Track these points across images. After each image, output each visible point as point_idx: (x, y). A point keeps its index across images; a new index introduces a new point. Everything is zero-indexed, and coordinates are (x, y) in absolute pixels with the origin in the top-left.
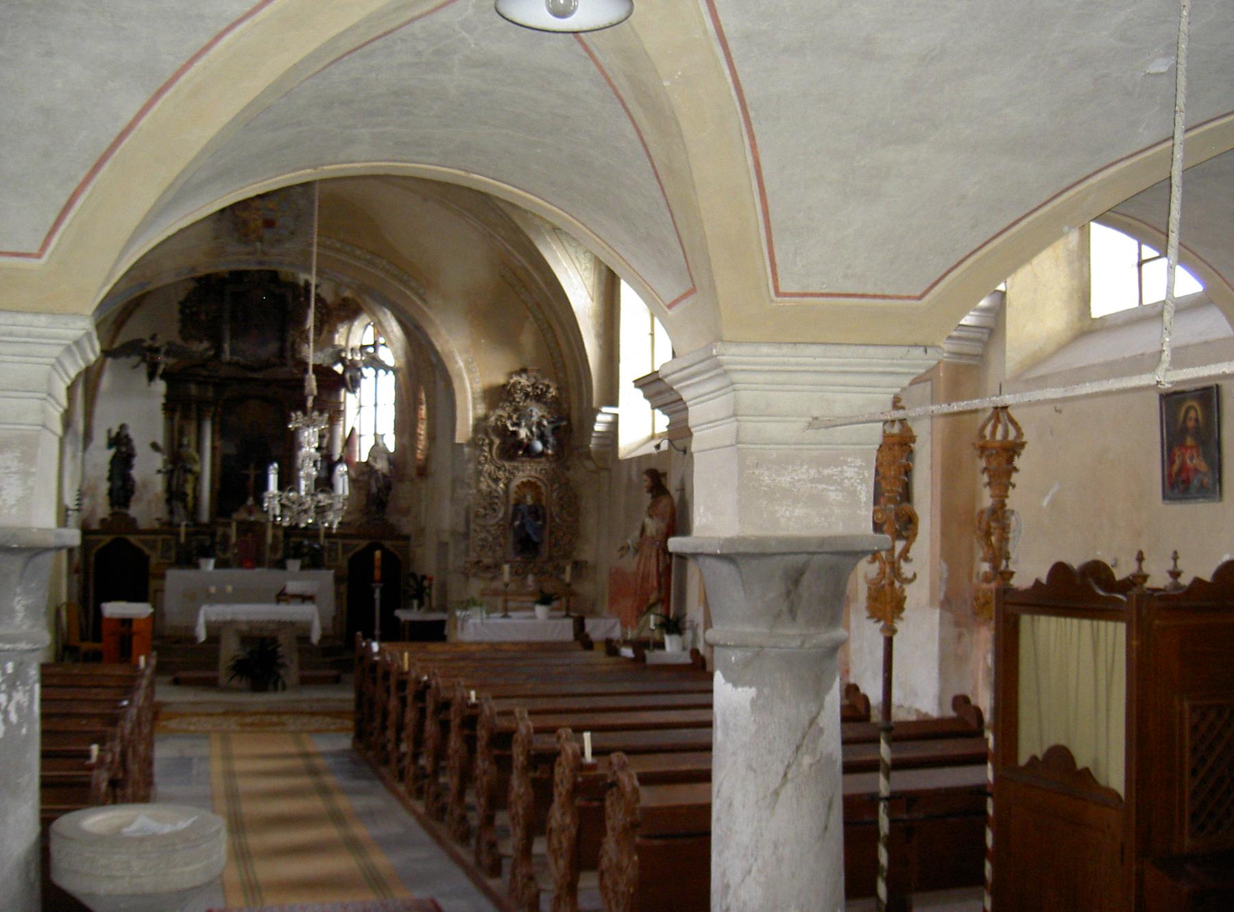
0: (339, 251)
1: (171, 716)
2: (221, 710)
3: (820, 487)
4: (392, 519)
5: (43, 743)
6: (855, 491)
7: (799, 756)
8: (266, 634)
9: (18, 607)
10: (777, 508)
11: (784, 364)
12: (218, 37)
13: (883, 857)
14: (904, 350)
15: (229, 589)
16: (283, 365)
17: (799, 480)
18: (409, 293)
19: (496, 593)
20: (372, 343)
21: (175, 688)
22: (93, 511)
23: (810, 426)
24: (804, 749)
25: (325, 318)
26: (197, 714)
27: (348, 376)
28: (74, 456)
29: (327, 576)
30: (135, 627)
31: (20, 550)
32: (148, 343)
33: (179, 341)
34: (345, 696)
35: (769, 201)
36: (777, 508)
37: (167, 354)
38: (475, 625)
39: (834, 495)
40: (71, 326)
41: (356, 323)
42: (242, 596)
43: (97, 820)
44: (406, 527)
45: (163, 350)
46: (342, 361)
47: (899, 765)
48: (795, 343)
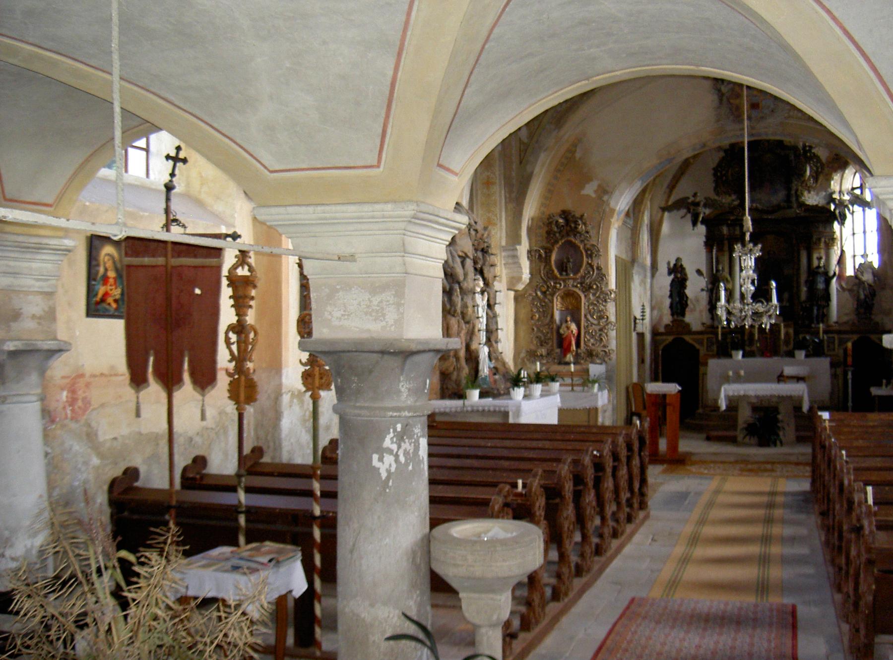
1: (694, 463)
2: (732, 459)
9: (403, 390)
12: (409, 14)
15: (742, 373)
16: (790, 207)
20: (859, 185)
22: (661, 318)
25: (820, 170)
27: (837, 212)
28: (643, 282)
29: (823, 364)
30: (668, 401)
32: (691, 199)
33: (714, 196)
34: (807, 450)
37: (705, 206)
40: (406, 209)
41: (847, 171)
42: (753, 377)
45: (702, 203)
46: (833, 200)
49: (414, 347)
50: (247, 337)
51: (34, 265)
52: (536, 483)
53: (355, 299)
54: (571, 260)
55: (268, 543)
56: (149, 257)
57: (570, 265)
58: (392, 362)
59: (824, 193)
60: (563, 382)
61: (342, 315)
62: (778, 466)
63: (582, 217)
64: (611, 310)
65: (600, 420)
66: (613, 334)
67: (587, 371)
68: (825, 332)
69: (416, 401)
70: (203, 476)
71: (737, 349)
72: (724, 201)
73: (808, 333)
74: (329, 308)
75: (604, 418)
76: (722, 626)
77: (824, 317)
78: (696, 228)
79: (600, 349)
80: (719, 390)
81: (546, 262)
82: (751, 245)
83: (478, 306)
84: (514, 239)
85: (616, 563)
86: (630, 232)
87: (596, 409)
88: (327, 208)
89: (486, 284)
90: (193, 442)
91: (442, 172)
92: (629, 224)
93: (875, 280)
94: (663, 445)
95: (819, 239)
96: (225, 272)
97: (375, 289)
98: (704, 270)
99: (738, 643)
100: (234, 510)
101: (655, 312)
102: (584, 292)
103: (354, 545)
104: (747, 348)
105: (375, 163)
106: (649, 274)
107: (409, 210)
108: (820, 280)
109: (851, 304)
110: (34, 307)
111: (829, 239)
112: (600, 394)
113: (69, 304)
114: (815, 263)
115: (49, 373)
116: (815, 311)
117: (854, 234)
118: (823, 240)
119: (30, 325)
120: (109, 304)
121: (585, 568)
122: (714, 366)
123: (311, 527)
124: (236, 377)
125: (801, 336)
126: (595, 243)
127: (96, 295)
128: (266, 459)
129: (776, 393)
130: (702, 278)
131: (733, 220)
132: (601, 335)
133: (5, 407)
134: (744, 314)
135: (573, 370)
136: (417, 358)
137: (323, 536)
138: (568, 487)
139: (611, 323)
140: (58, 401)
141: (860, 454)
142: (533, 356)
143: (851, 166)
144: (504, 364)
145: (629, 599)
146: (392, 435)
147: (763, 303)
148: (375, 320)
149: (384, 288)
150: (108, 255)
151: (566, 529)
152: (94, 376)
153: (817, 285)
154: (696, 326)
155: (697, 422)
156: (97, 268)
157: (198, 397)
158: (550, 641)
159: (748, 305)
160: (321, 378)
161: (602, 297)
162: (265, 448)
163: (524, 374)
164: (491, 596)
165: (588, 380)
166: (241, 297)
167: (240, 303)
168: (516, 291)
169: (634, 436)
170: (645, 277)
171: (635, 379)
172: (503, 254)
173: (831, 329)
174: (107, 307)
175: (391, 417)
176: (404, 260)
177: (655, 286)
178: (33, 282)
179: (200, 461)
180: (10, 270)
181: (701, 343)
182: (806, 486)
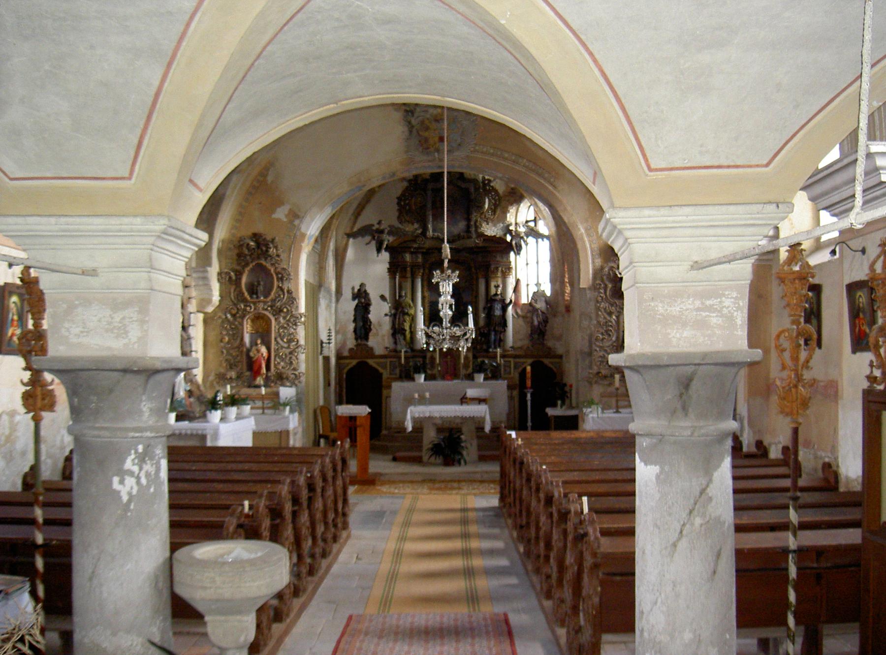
0: (493, 155)
1: (383, 483)
2: (420, 478)
3: (704, 314)
4: (550, 343)
5: (170, 498)
6: (732, 316)
7: (692, 518)
8: (454, 426)
9: (144, 409)
10: (669, 331)
11: (665, 222)
12: (188, 25)
13: (792, 596)
14: (760, 207)
15: (427, 395)
16: (470, 237)
17: (687, 310)
18: (542, 181)
19: (610, 395)
20: (533, 219)
21: (393, 464)
22: (344, 344)
23: (692, 268)
24: (695, 512)
26: (403, 482)
27: (514, 243)
28: (328, 306)
29: (501, 386)
30: (358, 423)
31: (138, 372)
32: (376, 227)
33: (396, 224)
34: (494, 468)
35: (623, 101)
36: (669, 331)
38: (593, 418)
39: (715, 320)
43: (206, 550)
44: (560, 350)
45: (386, 231)
46: (510, 232)
47: (804, 526)
48: (670, 206)
49: (159, 365)
52: (262, 503)
53: (95, 316)
57: (261, 288)
58: (138, 380)
59: (502, 225)
60: (254, 406)
63: (273, 241)
64: (301, 333)
65: (291, 443)
66: (302, 357)
67: (277, 394)
68: (503, 356)
69: (157, 421)
71: (419, 372)
72: (407, 229)
73: (487, 357)
74: (66, 325)
75: (295, 440)
76: (442, 637)
77: (500, 342)
79: (290, 372)
81: (236, 284)
82: (450, 271)
86: (317, 257)
87: (288, 432)
88: (70, 220)
91: (191, 188)
95: (497, 268)
97: (117, 306)
98: (387, 295)
102: (274, 315)
103: (93, 572)
104: (429, 372)
105: (127, 175)
106: (334, 299)
107: (160, 225)
108: (498, 306)
109: (525, 330)
112: (291, 416)
114: (493, 291)
117: (527, 264)
118: (500, 269)
121: (301, 588)
122: (398, 388)
123: (33, 557)
125: (479, 360)
129: (459, 414)
130: (386, 303)
131: (415, 248)
132: (291, 358)
136: (159, 377)
137: (46, 565)
138: (288, 507)
139: (300, 346)
141: (555, 469)
142: (222, 379)
143: (526, 200)
144: (198, 387)
145: (347, 616)
147: (460, 327)
148: (117, 337)
149: (127, 304)
153: (494, 312)
154: (379, 350)
159: (446, 328)
160: (43, 399)
161: (292, 320)
164: (238, 617)
168: (205, 313)
170: (330, 301)
171: (321, 403)
175: (133, 437)
176: (149, 277)
177: (339, 311)
181: (385, 368)
182: (494, 502)
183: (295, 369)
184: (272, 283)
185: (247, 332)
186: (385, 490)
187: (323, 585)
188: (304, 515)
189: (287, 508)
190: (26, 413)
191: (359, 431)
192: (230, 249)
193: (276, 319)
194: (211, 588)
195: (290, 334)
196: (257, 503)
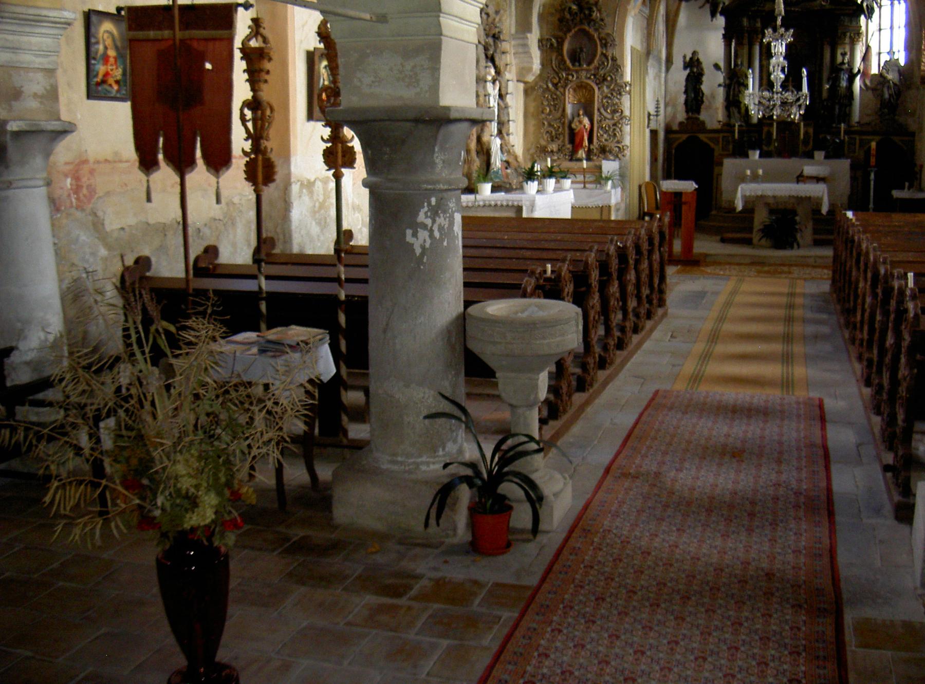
2: (748, 261)
9: (437, 161)
15: (760, 172)
22: (674, 117)
26: (730, 264)
27: (865, 5)
28: (658, 76)
29: (844, 165)
30: (683, 200)
34: (828, 252)
42: (770, 177)
44: (913, 127)
50: (263, 114)
51: (34, 40)
52: (565, 269)
54: (585, 50)
55: (293, 327)
56: (153, 30)
57: (583, 55)
60: (575, 179)
61: (373, 82)
62: (795, 268)
63: (596, 4)
67: (600, 168)
70: (217, 266)
71: (754, 149)
74: (359, 75)
76: (749, 417)
77: (846, 116)
78: (714, 19)
80: (735, 191)
82: (783, 29)
83: (489, 95)
84: (524, 26)
85: (637, 358)
86: (645, 22)
89: (498, 72)
90: (201, 234)
92: (645, 13)
93: (900, 79)
94: (677, 246)
95: (844, 34)
96: (238, 43)
99: (767, 432)
100: (255, 296)
101: (669, 109)
102: (597, 84)
103: (387, 325)
106: (664, 69)
108: (844, 77)
110: (35, 85)
111: (854, 34)
112: (613, 191)
113: (69, 85)
114: (839, 59)
115: (52, 158)
116: (837, 110)
117: (880, 30)
118: (848, 34)
119: (34, 104)
120: (110, 85)
122: (730, 165)
124: (253, 156)
126: (610, 32)
127: (97, 75)
128: (277, 251)
129: (794, 194)
132: (614, 130)
133: (10, 193)
134: (772, 103)
135: (585, 166)
138: (595, 275)
139: (625, 117)
140: (62, 188)
144: (516, 158)
146: (426, 209)
150: (107, 32)
151: (592, 318)
152: (98, 162)
153: (840, 83)
155: (712, 224)
156: (96, 46)
157: (213, 179)
158: (576, 429)
159: (777, 93)
162: (276, 238)
163: (537, 167)
165: (601, 176)
166: (256, 71)
167: (255, 77)
168: (525, 83)
169: (655, 229)
170: (660, 71)
172: (513, 43)
173: (853, 129)
174: (108, 88)
175: (426, 189)
178: (33, 58)
179: (211, 251)
180: (9, 45)
182: (826, 287)
183: (618, 142)
184: (596, 51)
185: (569, 103)
186: (709, 271)
187: (632, 360)
188: (613, 285)
189: (593, 276)
190: (327, 170)
191: (684, 208)
192: (552, 14)
193: (599, 88)
194: (500, 343)
195: (614, 105)
196: (560, 267)
